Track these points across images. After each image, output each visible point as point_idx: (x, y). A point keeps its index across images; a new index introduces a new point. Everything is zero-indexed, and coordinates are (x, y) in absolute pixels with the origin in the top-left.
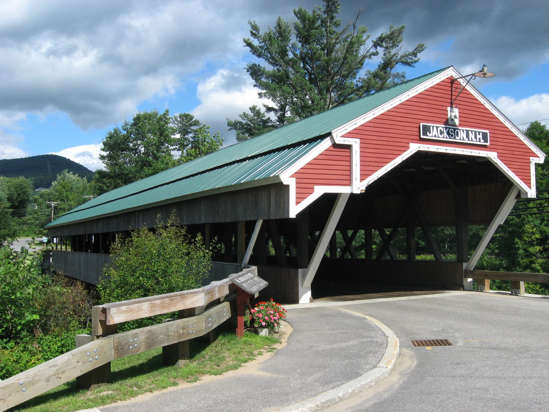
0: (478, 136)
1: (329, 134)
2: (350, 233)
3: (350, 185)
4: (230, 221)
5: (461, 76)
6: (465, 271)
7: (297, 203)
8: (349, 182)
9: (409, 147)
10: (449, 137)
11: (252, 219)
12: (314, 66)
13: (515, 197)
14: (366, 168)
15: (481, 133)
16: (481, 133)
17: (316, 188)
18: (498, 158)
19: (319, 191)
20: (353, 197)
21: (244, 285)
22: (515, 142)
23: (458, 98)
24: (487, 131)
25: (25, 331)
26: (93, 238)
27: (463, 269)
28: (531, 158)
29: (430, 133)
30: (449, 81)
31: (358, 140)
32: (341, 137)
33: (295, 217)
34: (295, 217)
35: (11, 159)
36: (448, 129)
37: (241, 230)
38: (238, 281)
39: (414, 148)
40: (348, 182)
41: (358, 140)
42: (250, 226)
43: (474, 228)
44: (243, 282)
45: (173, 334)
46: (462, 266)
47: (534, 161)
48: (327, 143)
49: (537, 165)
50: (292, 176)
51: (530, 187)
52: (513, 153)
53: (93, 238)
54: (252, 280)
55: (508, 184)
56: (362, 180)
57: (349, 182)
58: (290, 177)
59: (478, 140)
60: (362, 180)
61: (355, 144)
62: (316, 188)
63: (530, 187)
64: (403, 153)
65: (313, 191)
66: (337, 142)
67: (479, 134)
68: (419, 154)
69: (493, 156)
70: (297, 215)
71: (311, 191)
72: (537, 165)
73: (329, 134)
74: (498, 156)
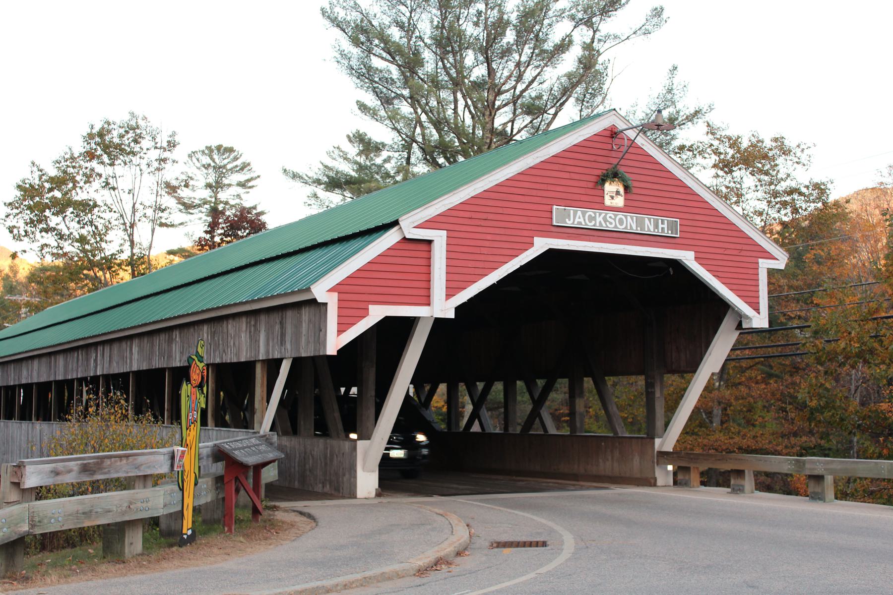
0: (660, 226)
1: (396, 223)
3: (429, 304)
4: (245, 360)
5: (631, 126)
6: (657, 452)
7: (340, 332)
8: (427, 301)
9: (533, 244)
10: (606, 224)
12: (426, 86)
13: (735, 327)
14: (456, 277)
15: (666, 222)
16: (666, 222)
17: (372, 308)
18: (695, 260)
19: (377, 313)
20: (439, 323)
21: (236, 452)
22: (731, 234)
23: (622, 162)
24: (678, 220)
25: (7, 325)
26: (22, 398)
27: (654, 448)
28: (760, 261)
29: (569, 220)
31: (444, 233)
32: (414, 227)
33: (335, 353)
34: (335, 353)
36: (603, 215)
37: (260, 374)
38: (227, 446)
39: (541, 245)
40: (424, 300)
41: (444, 233)
42: (273, 366)
44: (235, 449)
45: (115, 510)
46: (654, 443)
47: (764, 265)
48: (390, 238)
49: (771, 272)
50: (331, 290)
51: (757, 310)
52: (725, 253)
55: (722, 307)
56: (449, 296)
57: (427, 301)
58: (327, 291)
59: (660, 231)
60: (449, 296)
61: (439, 238)
62: (372, 308)
63: (757, 310)
64: (522, 253)
65: (368, 314)
69: (688, 258)
70: (338, 351)
71: (365, 313)
72: (771, 272)
73: (396, 223)
74: (696, 259)
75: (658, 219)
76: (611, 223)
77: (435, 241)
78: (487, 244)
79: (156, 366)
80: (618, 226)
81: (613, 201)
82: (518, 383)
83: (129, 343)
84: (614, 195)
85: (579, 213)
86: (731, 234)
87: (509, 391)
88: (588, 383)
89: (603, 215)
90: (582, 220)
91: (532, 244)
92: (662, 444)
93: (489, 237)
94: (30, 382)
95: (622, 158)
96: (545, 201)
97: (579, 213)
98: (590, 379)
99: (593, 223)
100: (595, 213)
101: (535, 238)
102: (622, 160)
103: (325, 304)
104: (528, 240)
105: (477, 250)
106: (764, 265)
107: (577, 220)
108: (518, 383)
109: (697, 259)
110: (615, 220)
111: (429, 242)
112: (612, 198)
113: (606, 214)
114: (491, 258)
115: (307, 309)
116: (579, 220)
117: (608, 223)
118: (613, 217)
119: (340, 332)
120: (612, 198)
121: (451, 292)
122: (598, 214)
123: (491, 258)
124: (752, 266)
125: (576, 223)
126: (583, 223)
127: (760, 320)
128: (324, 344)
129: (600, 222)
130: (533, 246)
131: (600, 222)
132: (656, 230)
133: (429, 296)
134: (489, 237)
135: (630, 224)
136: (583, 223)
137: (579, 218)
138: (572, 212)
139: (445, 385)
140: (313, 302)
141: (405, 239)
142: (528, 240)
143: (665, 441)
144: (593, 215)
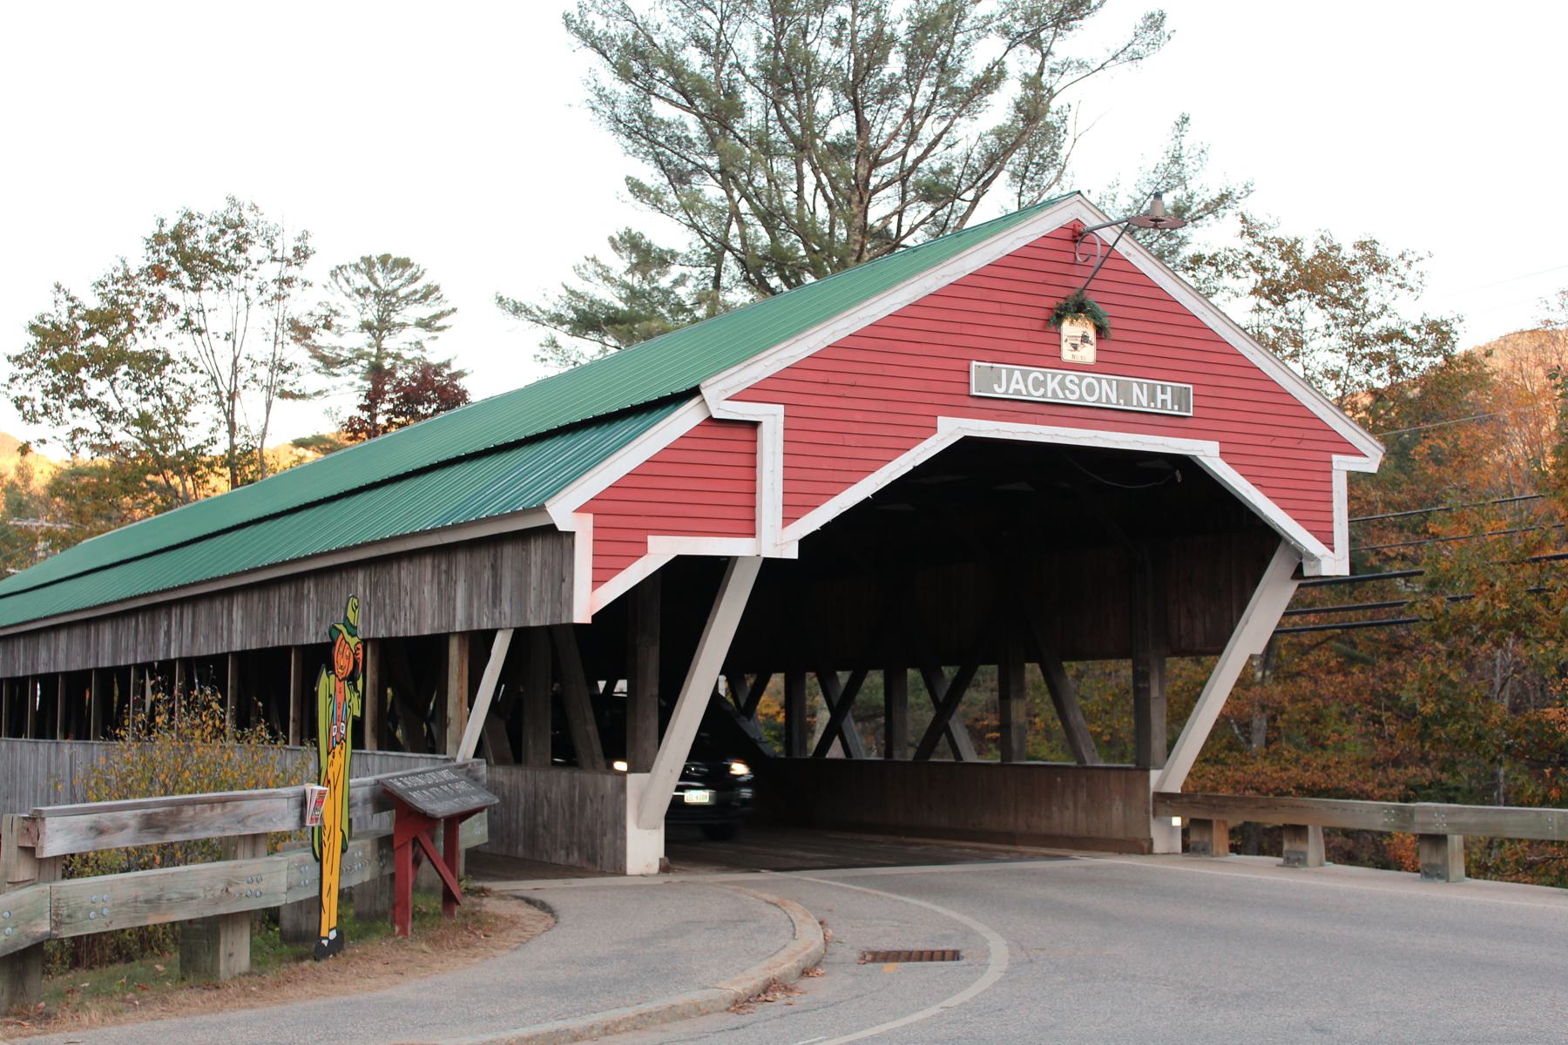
0: (1160, 397)
1: (695, 392)
2: (843, 677)
3: (753, 535)
4: (429, 633)
5: (1108, 221)
6: (1154, 793)
7: (597, 582)
8: (749, 529)
9: (936, 428)
10: (1064, 394)
11: (486, 624)
13: (1291, 575)
14: (801, 487)
15: (1169, 389)
16: (1169, 389)
17: (652, 540)
18: (1221, 457)
19: (661, 550)
20: (771, 568)
21: (415, 795)
22: (1283, 410)
26: (38, 699)
27: (1149, 787)
28: (1335, 458)
29: (1000, 387)
30: (1068, 234)
31: (779, 410)
32: (727, 399)
33: (588, 620)
34: (588, 620)
35: (522, 386)
36: (1059, 377)
37: (456, 656)
38: (399, 784)
39: (950, 431)
40: (744, 527)
41: (779, 410)
42: (479, 643)
43: (1180, 667)
44: (413, 789)
46: (1148, 779)
47: (1342, 465)
48: (685, 419)
49: (1354, 479)
50: (582, 510)
51: (1330, 545)
52: (1273, 444)
53: (432, 705)
54: (446, 788)
55: (1268, 539)
56: (788, 520)
57: (749, 529)
58: (575, 511)
59: (1159, 406)
60: (788, 520)
61: (771, 418)
62: (652, 540)
63: (1330, 545)
64: (916, 445)
65: (646, 552)
66: (715, 416)
67: (1163, 392)
68: (680, 562)
69: (1207, 453)
70: (594, 617)
71: (640, 550)
72: (1354, 479)
73: (695, 392)
74: (1223, 454)
75: (1155, 385)
76: (1073, 392)
77: (764, 424)
78: (855, 428)
79: (273, 643)
80: (1086, 396)
81: (1076, 353)
82: (910, 672)
83: (226, 603)
84: (1079, 342)
85: (1017, 375)
86: (1283, 410)
87: (894, 687)
88: (1033, 672)
89: (1059, 377)
90: (1021, 386)
91: (934, 429)
92: (1162, 780)
93: (858, 417)
94: (52, 671)
95: (1092, 278)
96: (956, 353)
97: (1017, 375)
98: (1037, 666)
99: (1042, 391)
100: (1044, 374)
101: (940, 418)
102: (1092, 282)
103: (572, 534)
104: (927, 421)
105: (838, 439)
106: (1342, 465)
107: (1013, 386)
108: (910, 672)
109: (1223, 454)
110: (1079, 386)
111: (754, 425)
112: (1075, 347)
113: (1065, 376)
114: (862, 454)
115: (540, 542)
116: (1017, 387)
117: (1067, 392)
118: (1077, 381)
119: (597, 582)
120: (1075, 347)
121: (791, 513)
122: (1049, 376)
123: (862, 454)
124: (1321, 467)
125: (1011, 391)
126: (1024, 392)
127: (1334, 563)
128: (569, 604)
129: (1054, 391)
130: (936, 432)
131: (1054, 391)
132: (1152, 405)
133: (754, 520)
134: (858, 417)
135: (1107, 394)
136: (1024, 392)
137: (1017, 383)
138: (1004, 372)
139: (781, 676)
140: (550, 530)
141: (711, 420)
142: (927, 421)
143: (1167, 775)
144: (1042, 378)
